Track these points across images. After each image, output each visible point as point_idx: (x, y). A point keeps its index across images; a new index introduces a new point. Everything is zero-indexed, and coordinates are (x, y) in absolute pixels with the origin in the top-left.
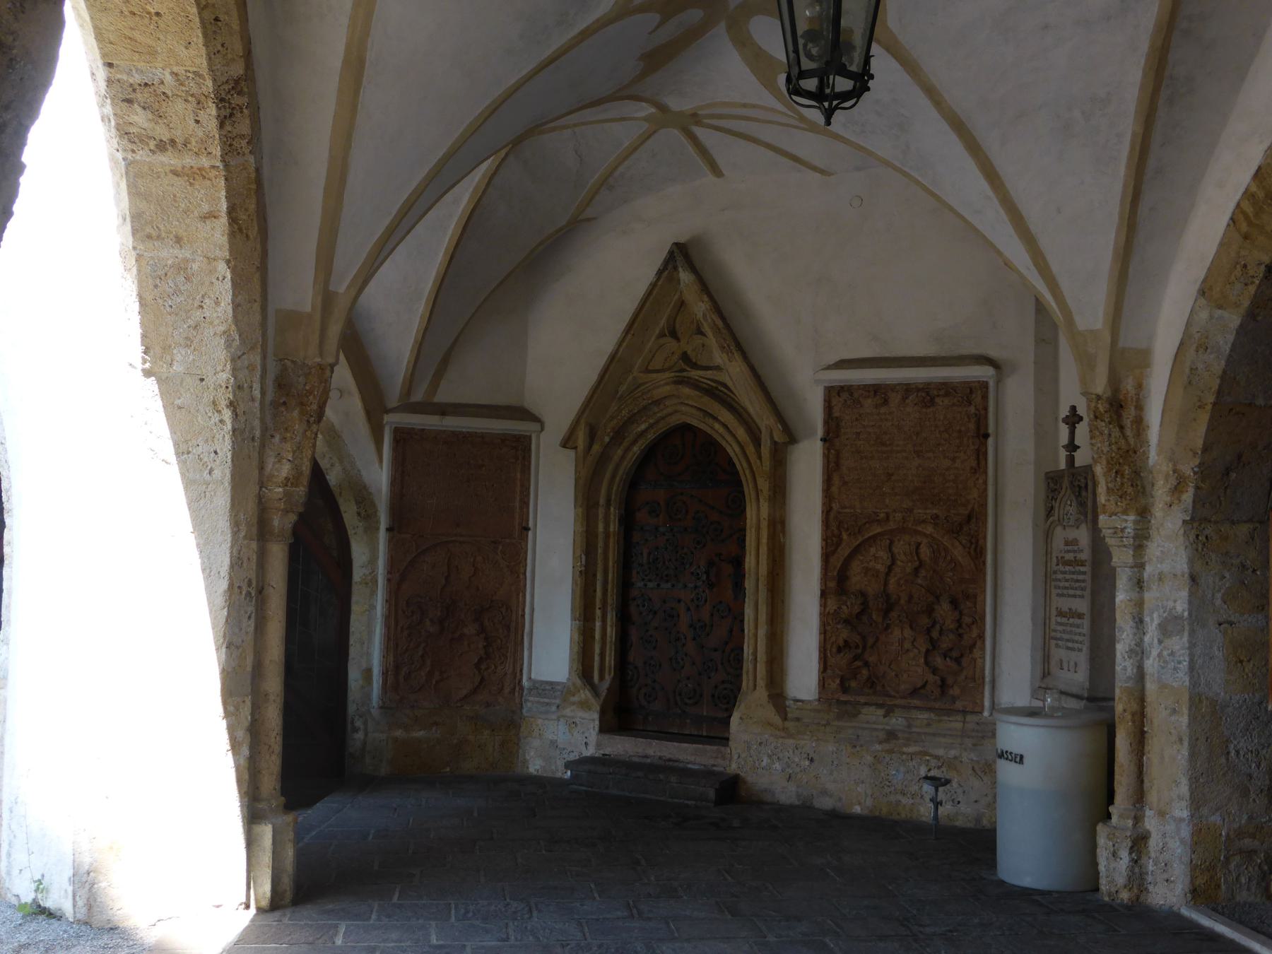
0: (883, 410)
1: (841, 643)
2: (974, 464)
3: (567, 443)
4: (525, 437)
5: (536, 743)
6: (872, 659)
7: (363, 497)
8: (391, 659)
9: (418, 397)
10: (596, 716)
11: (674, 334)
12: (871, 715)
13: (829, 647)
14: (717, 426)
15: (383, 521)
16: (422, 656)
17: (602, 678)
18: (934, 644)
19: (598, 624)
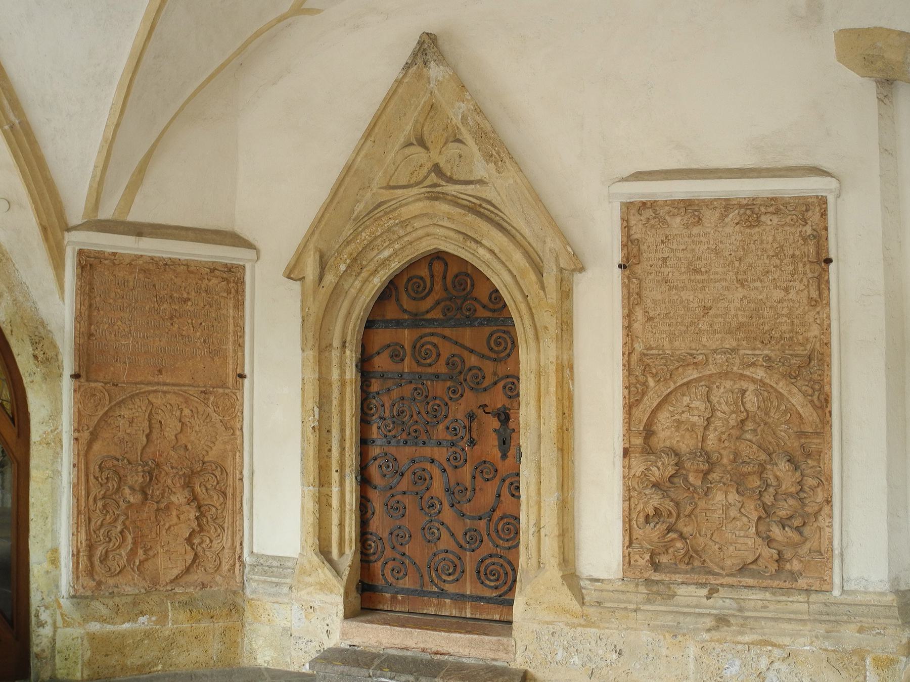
0: (695, 231)
1: (651, 512)
2: (814, 294)
3: (292, 273)
4: (238, 266)
5: (265, 630)
6: (687, 530)
7: (41, 340)
8: (83, 536)
9: (107, 212)
10: (340, 600)
11: (422, 143)
12: (690, 594)
13: (634, 516)
14: (481, 251)
15: (68, 366)
16: (122, 532)
17: (341, 553)
18: (767, 511)
19: (335, 489)
